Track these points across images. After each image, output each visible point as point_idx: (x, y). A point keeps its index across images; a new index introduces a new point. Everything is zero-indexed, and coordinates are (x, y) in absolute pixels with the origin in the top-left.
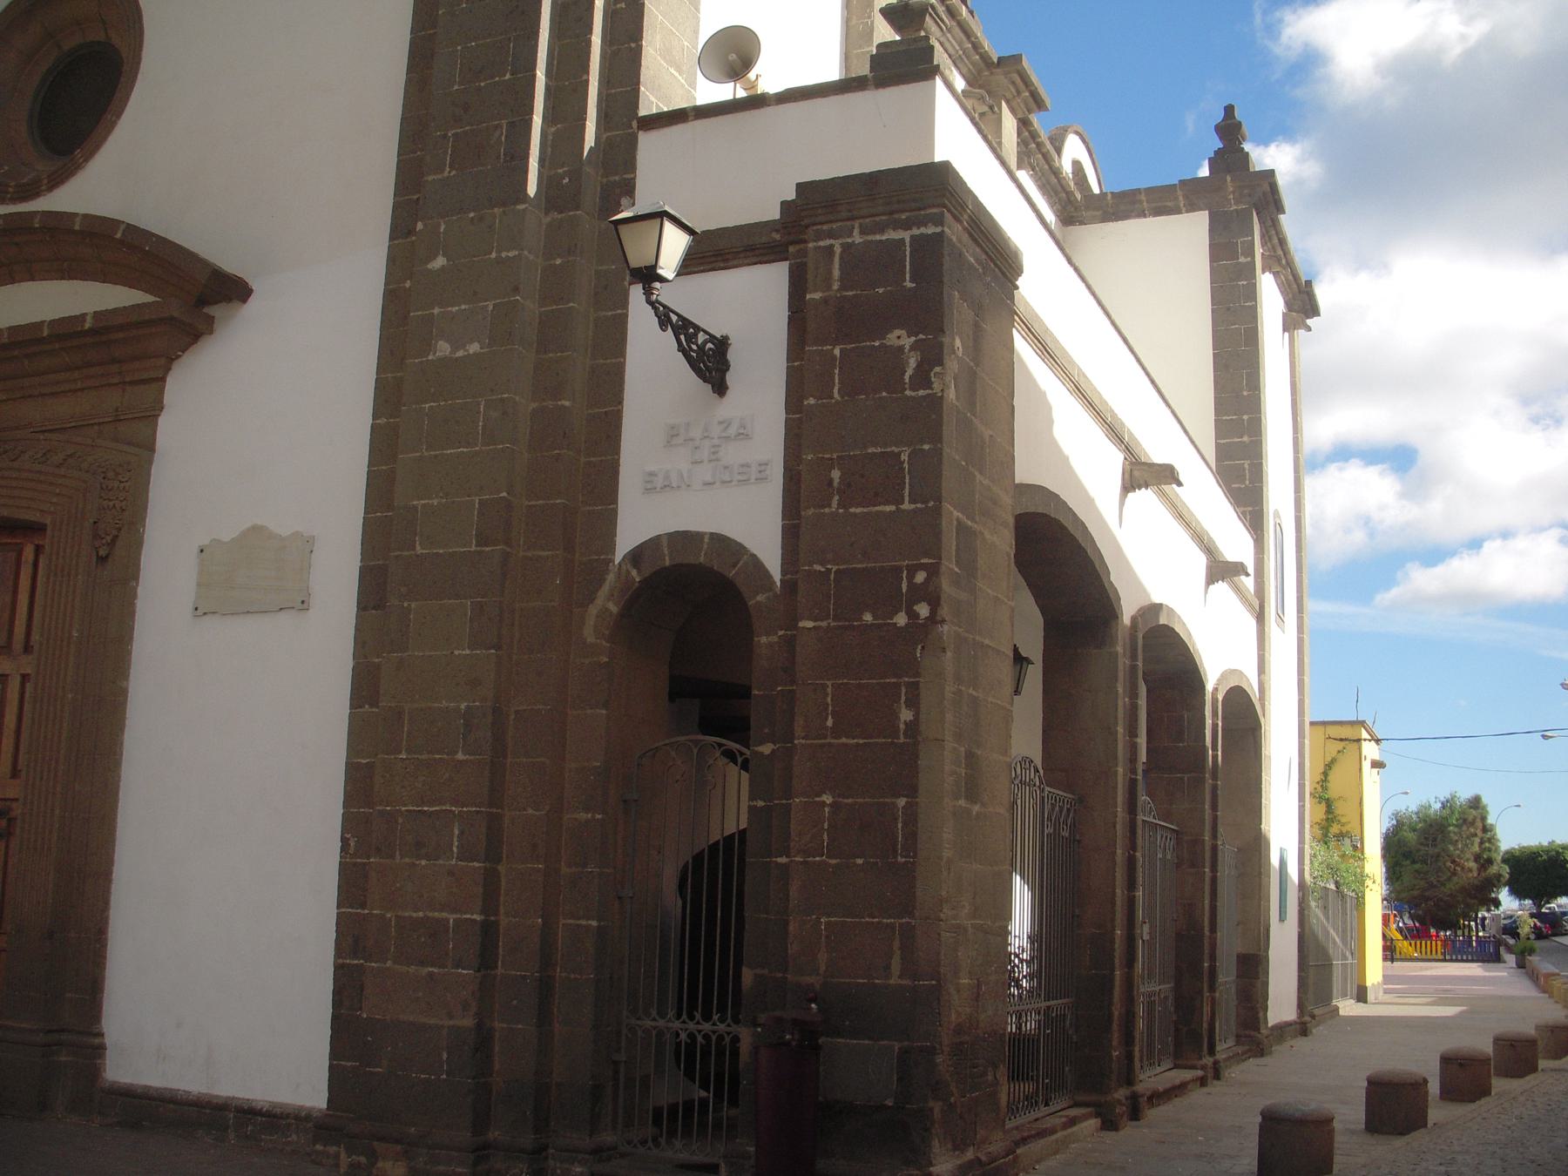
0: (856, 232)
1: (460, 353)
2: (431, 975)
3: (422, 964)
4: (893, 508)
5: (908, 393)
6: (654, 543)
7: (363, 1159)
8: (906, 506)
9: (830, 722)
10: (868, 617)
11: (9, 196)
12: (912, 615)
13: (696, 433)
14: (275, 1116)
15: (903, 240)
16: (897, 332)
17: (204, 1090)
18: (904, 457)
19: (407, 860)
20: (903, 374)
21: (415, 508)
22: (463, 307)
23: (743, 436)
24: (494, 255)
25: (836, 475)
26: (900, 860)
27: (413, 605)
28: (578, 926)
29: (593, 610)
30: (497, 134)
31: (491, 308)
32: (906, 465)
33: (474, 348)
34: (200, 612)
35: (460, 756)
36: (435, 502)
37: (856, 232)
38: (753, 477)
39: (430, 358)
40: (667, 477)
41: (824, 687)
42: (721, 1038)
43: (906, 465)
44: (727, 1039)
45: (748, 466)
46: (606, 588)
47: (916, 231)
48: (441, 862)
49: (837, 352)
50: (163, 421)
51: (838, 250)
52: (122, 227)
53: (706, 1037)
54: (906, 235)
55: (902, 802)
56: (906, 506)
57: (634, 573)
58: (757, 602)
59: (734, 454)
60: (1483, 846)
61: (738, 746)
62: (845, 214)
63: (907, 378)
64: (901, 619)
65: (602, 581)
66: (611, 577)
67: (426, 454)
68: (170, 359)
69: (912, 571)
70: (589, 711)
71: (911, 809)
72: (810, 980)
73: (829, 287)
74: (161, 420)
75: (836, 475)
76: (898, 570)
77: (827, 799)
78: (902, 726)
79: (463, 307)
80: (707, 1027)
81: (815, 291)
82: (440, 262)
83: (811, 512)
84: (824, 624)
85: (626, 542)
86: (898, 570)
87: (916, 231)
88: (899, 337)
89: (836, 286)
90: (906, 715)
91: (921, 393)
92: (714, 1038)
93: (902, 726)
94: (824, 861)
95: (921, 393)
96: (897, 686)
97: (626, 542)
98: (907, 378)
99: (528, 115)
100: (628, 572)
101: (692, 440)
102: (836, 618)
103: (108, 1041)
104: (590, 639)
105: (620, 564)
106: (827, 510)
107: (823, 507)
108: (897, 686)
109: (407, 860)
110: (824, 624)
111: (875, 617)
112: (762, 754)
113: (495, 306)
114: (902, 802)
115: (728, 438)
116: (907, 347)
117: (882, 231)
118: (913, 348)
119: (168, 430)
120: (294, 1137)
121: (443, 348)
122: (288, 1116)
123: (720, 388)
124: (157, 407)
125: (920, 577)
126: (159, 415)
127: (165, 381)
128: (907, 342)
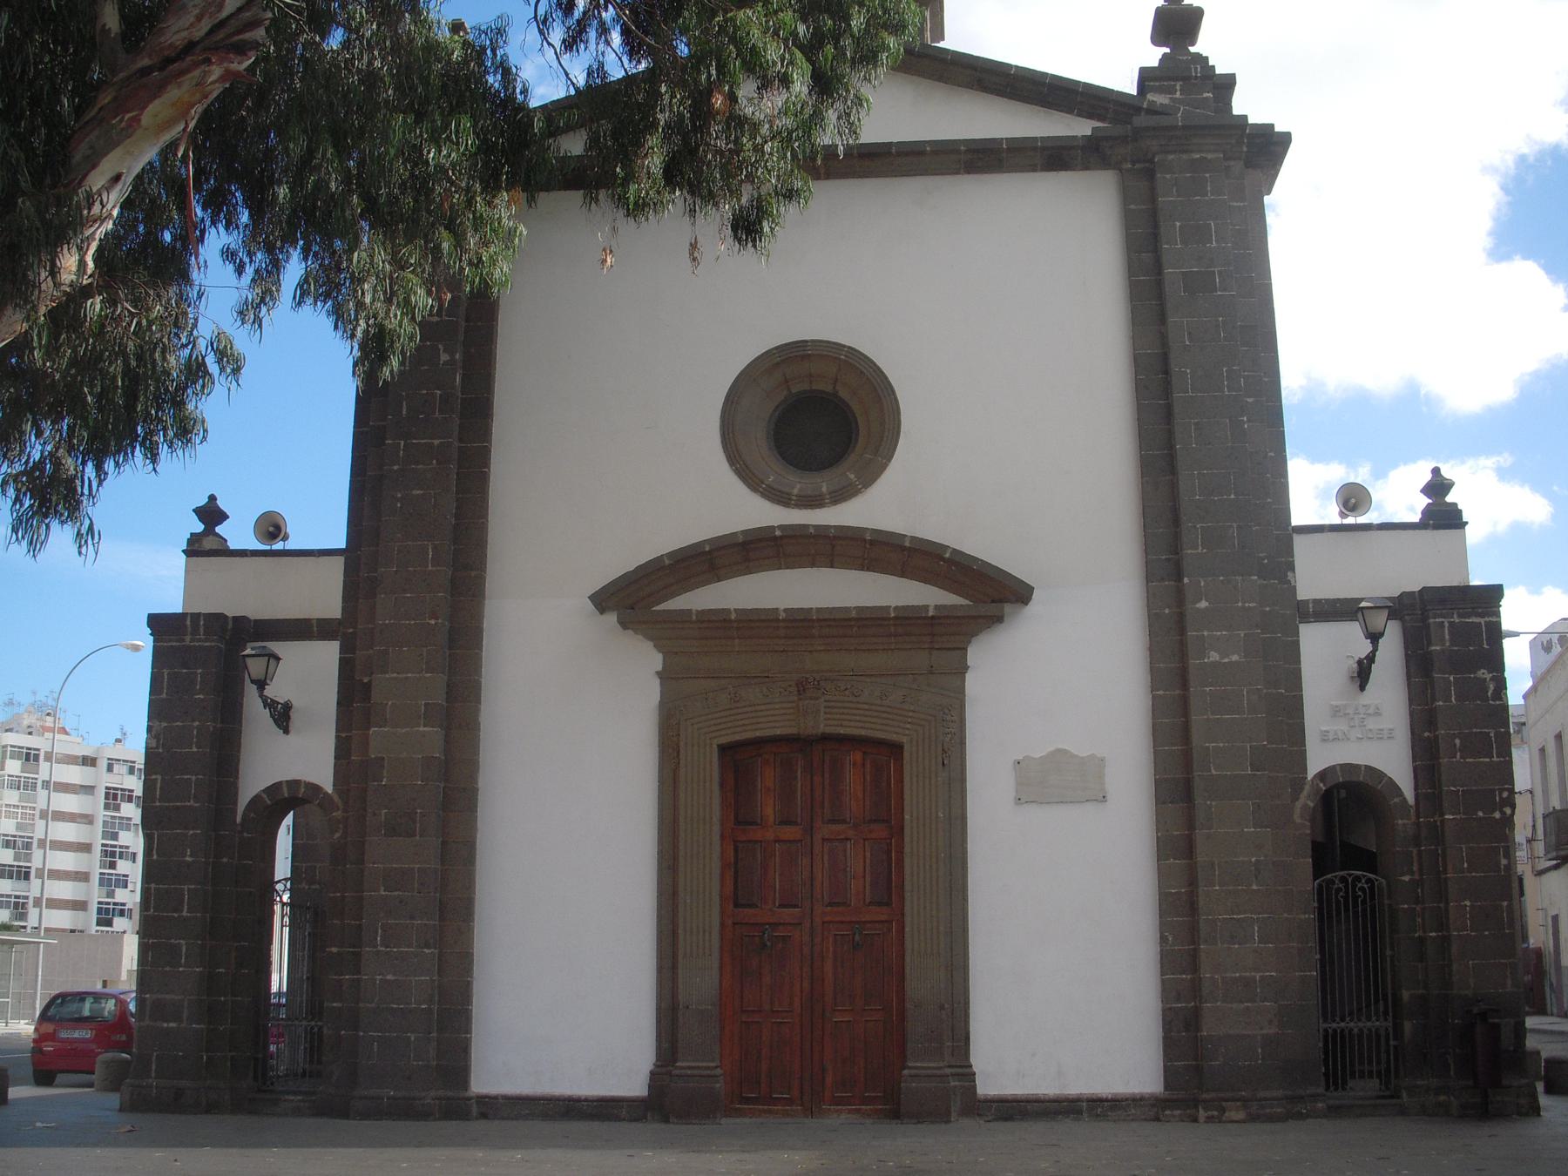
0: (1455, 616)
1: (1226, 660)
2: (1248, 1008)
3: (1242, 1002)
4: (1488, 760)
5: (1491, 702)
6: (1331, 769)
7: (1215, 1113)
8: (1495, 759)
9: (1466, 865)
10: (1480, 814)
11: (793, 502)
12: (1503, 813)
13: (1350, 711)
14: (1118, 1101)
15: (1480, 623)
16: (1482, 671)
17: (1057, 1092)
18: (1492, 735)
19: (1225, 946)
20: (1487, 692)
21: (1208, 748)
22: (1224, 633)
23: (1377, 714)
24: (1240, 604)
25: (1457, 741)
26: (1507, 931)
27: (1213, 803)
28: (1306, 976)
29: (1299, 804)
30: (1231, 531)
31: (1242, 635)
32: (1493, 739)
33: (1235, 658)
34: (1022, 801)
35: (1255, 887)
36: (1221, 745)
37: (1455, 616)
38: (1385, 737)
39: (1206, 661)
40: (1336, 734)
41: (1461, 849)
42: (1342, 1030)
43: (1493, 739)
44: (1347, 1032)
45: (1382, 730)
46: (1305, 793)
47: (1487, 619)
48: (1248, 945)
49: (1452, 678)
50: (969, 676)
51: (1447, 624)
52: (950, 550)
53: (1370, 1030)
54: (1482, 621)
55: (1505, 904)
56: (1495, 759)
57: (1321, 785)
58: (1395, 803)
59: (1372, 724)
60: (347, 761)
61: (1346, 872)
62: (1449, 606)
63: (1489, 694)
64: (1497, 815)
65: (1302, 789)
66: (1307, 788)
67: (1211, 717)
68: (974, 634)
69: (1501, 791)
70: (1302, 860)
71: (1510, 907)
72: (1466, 992)
73: (1444, 645)
74: (967, 675)
75: (1457, 741)
76: (1495, 790)
77: (1468, 903)
78: (1502, 867)
79: (1224, 633)
80: (1369, 1024)
81: (1437, 645)
82: (1203, 604)
83: (1446, 760)
84: (1458, 817)
85: (1313, 768)
86: (1495, 790)
87: (1487, 619)
88: (1483, 674)
89: (1448, 644)
90: (1504, 862)
91: (1498, 703)
92: (1373, 1030)
93: (1502, 867)
94: (1467, 934)
95: (1498, 703)
96: (1498, 848)
97: (1313, 768)
98: (1489, 694)
99: (1495, 607)
100: (1317, 784)
101: (1348, 714)
102: (1464, 814)
103: (975, 1069)
104: (1299, 821)
105: (1312, 780)
106: (1454, 760)
107: (1453, 758)
108: (1498, 848)
109: (1225, 946)
110: (1458, 817)
111: (1484, 813)
112: (1404, 881)
113: (1245, 635)
114: (1505, 904)
115: (1369, 714)
116: (1488, 679)
117: (1469, 618)
118: (1491, 679)
119: (973, 684)
120: (1133, 1111)
121: (1214, 656)
122: (1127, 1100)
123: (1362, 688)
124: (962, 669)
125: (1505, 794)
126: (965, 673)
127: (967, 650)
128: (1488, 676)
